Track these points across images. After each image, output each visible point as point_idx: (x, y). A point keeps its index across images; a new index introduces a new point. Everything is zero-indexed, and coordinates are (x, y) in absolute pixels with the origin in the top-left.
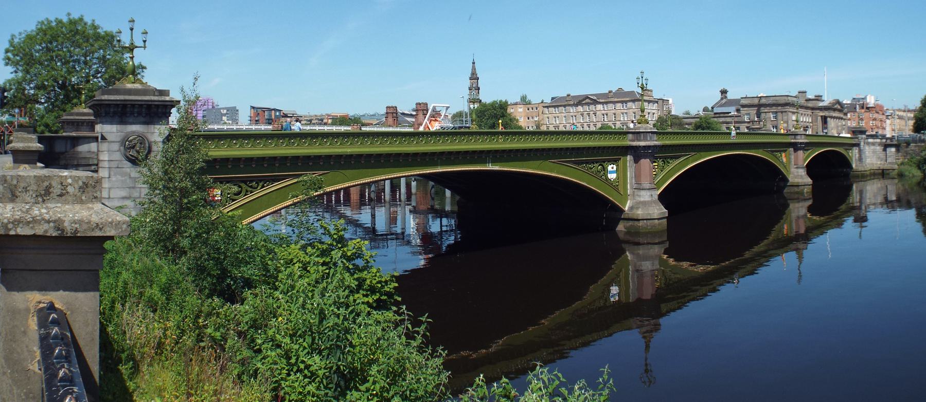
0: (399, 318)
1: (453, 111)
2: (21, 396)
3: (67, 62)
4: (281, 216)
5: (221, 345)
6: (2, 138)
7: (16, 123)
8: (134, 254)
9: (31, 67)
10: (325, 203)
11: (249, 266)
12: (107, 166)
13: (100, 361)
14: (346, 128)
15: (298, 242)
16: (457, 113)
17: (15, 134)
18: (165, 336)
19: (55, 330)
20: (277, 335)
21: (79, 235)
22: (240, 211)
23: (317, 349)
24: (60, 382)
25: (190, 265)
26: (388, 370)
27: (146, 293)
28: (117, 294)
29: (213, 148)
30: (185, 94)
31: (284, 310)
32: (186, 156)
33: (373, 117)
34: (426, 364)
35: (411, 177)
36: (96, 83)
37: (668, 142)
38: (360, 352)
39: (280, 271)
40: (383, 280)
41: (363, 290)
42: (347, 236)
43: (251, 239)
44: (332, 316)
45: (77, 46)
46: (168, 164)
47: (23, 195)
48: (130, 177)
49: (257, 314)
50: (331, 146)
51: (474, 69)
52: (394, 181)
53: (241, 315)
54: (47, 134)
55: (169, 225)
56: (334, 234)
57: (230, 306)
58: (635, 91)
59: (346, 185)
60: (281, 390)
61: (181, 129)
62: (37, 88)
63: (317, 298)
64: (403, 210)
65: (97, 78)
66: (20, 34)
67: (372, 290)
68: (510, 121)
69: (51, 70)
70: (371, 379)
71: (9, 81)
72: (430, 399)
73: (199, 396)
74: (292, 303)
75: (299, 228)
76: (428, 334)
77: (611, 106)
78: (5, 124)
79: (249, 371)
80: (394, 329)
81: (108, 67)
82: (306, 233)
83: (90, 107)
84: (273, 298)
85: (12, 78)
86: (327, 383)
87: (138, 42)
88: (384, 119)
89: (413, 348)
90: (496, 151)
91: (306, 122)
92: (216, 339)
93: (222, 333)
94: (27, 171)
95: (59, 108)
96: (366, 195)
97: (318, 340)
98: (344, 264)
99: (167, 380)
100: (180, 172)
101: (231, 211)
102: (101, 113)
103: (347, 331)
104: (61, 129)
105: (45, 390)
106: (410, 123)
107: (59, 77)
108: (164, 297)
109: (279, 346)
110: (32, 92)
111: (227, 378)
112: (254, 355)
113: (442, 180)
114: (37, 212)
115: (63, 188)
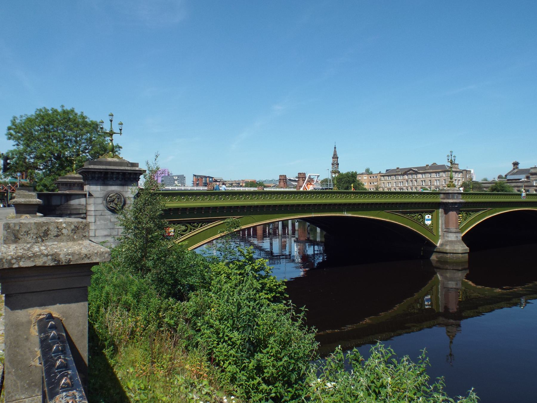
0: (287, 308)
1: (322, 178)
2: (24, 387)
3: (62, 141)
4: (213, 245)
5: (174, 329)
6: (6, 195)
7: (18, 183)
8: (114, 273)
9: (31, 142)
10: (241, 236)
11: (192, 277)
12: (93, 214)
13: (89, 349)
14: (254, 189)
15: (224, 261)
16: (324, 179)
17: (17, 192)
18: (136, 326)
19: (53, 333)
20: (211, 320)
21: (72, 263)
22: (186, 242)
23: (236, 328)
24: (57, 369)
25: (153, 278)
26: (281, 340)
27: (123, 299)
28: (101, 302)
29: (169, 202)
30: (150, 166)
31: (215, 303)
32: (150, 207)
33: (271, 182)
34: (304, 337)
35: (295, 220)
36: (84, 156)
37: (470, 200)
38: (263, 329)
39: (212, 280)
40: (278, 284)
41: (265, 290)
42: (255, 256)
43: (194, 259)
44: (246, 307)
45: (69, 130)
46: (137, 212)
47: (25, 237)
48: (111, 222)
49: (198, 307)
50: (245, 200)
51: (335, 151)
52: (285, 222)
53: (187, 309)
54: (45, 192)
55: (138, 253)
56: (247, 255)
57: (180, 303)
58: (446, 165)
59: (254, 224)
60: (214, 354)
61: (147, 189)
62: (36, 157)
63: (236, 296)
64: (290, 241)
65: (85, 153)
66: (21, 116)
67: (271, 290)
68: (358, 185)
69: (48, 146)
70: (270, 346)
71: (11, 151)
72: (307, 359)
73: (160, 362)
74: (220, 299)
75: (224, 252)
76: (305, 318)
77: (428, 175)
78: (8, 184)
79: (193, 343)
80: (284, 315)
81: (93, 146)
82: (229, 255)
83: (80, 173)
84: (208, 297)
85: (14, 150)
86: (242, 349)
87: (116, 129)
88: (278, 183)
89: (296, 326)
90: (350, 204)
91: (229, 185)
92: (171, 325)
93: (175, 321)
94: (26, 219)
95: (55, 173)
96: (266, 231)
97: (237, 322)
98: (253, 274)
99: (138, 355)
100: (146, 218)
101: (181, 242)
102: (88, 178)
103: (255, 316)
104: (57, 188)
105: (44, 377)
106: (294, 186)
107: (55, 151)
108: (136, 301)
109: (212, 327)
110: (32, 161)
111: (178, 349)
112: (196, 333)
113: (314, 221)
114: (37, 249)
115: (58, 230)
